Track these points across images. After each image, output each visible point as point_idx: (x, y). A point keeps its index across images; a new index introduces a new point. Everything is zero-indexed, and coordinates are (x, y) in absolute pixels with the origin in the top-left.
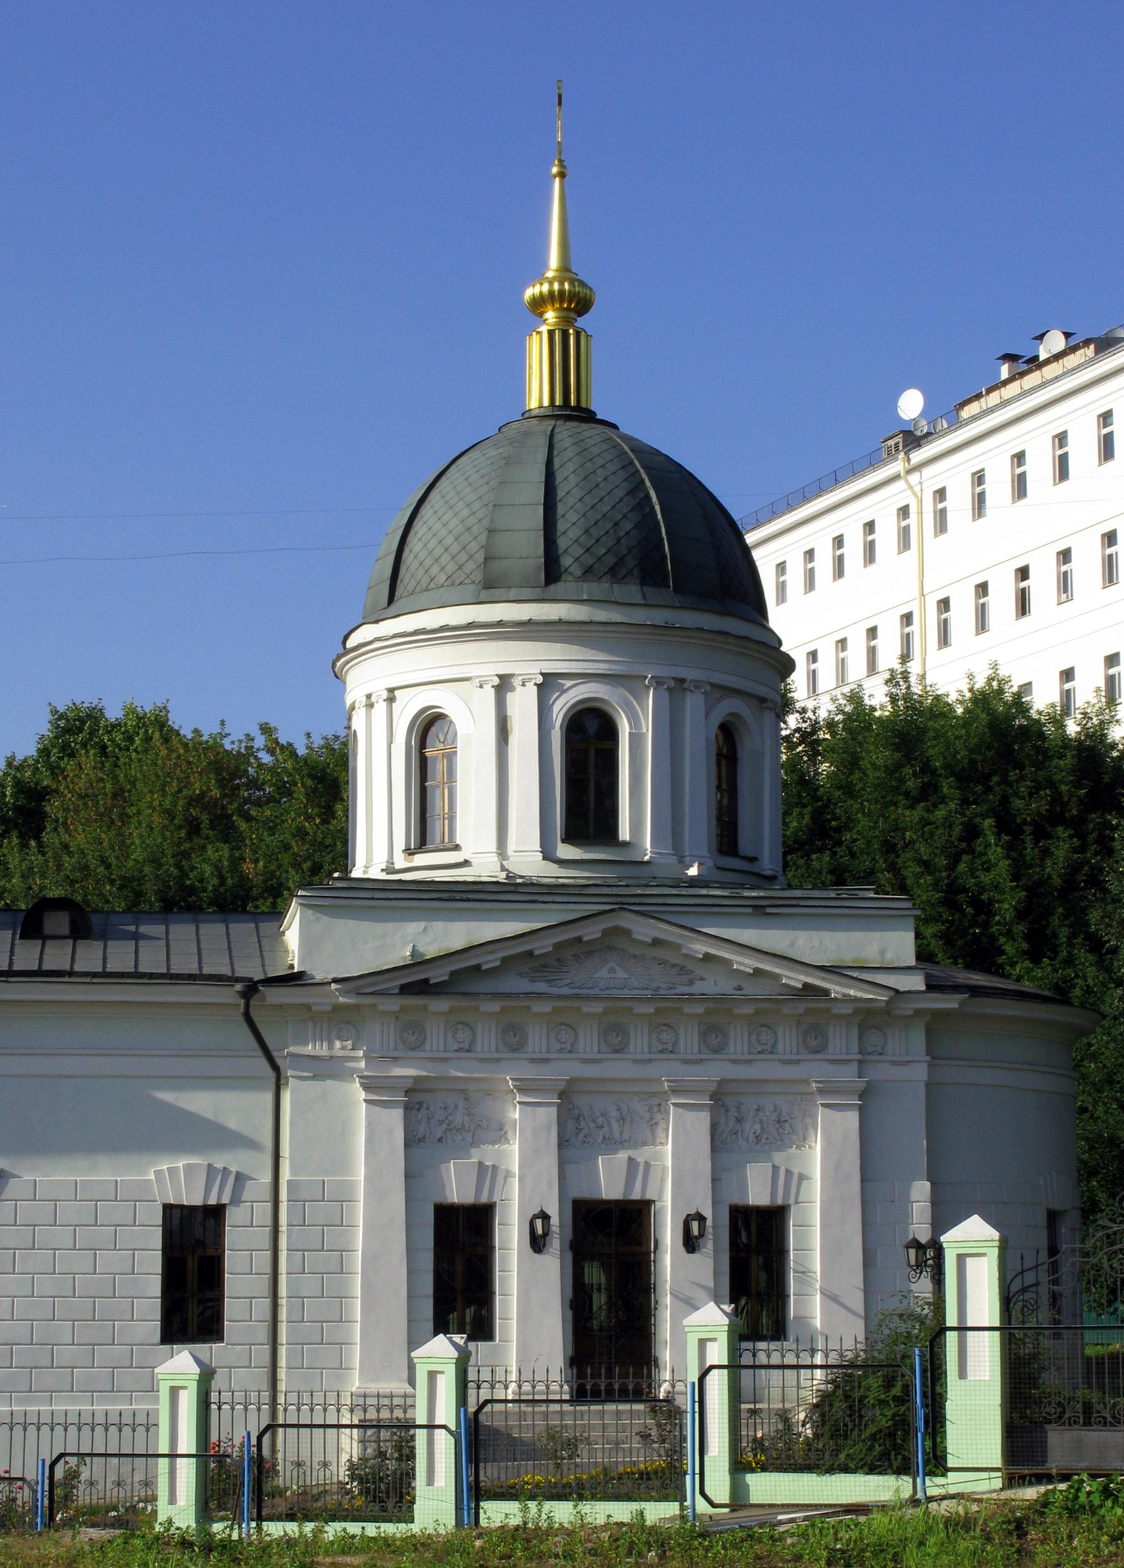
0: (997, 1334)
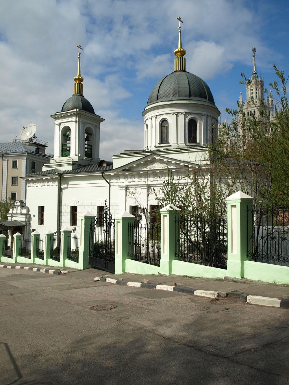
0: (124, 190)
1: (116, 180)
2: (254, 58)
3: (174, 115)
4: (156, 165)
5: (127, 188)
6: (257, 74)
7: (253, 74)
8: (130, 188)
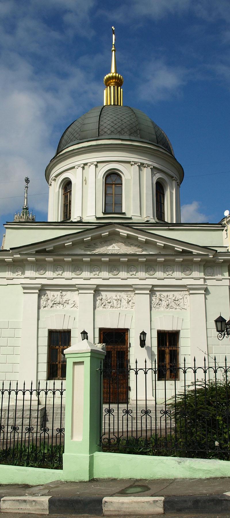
1: (14, 272)
2: (26, 190)
3: (136, 165)
4: (116, 246)
5: (42, 290)
6: (28, 210)
7: (23, 209)
8: (48, 292)
